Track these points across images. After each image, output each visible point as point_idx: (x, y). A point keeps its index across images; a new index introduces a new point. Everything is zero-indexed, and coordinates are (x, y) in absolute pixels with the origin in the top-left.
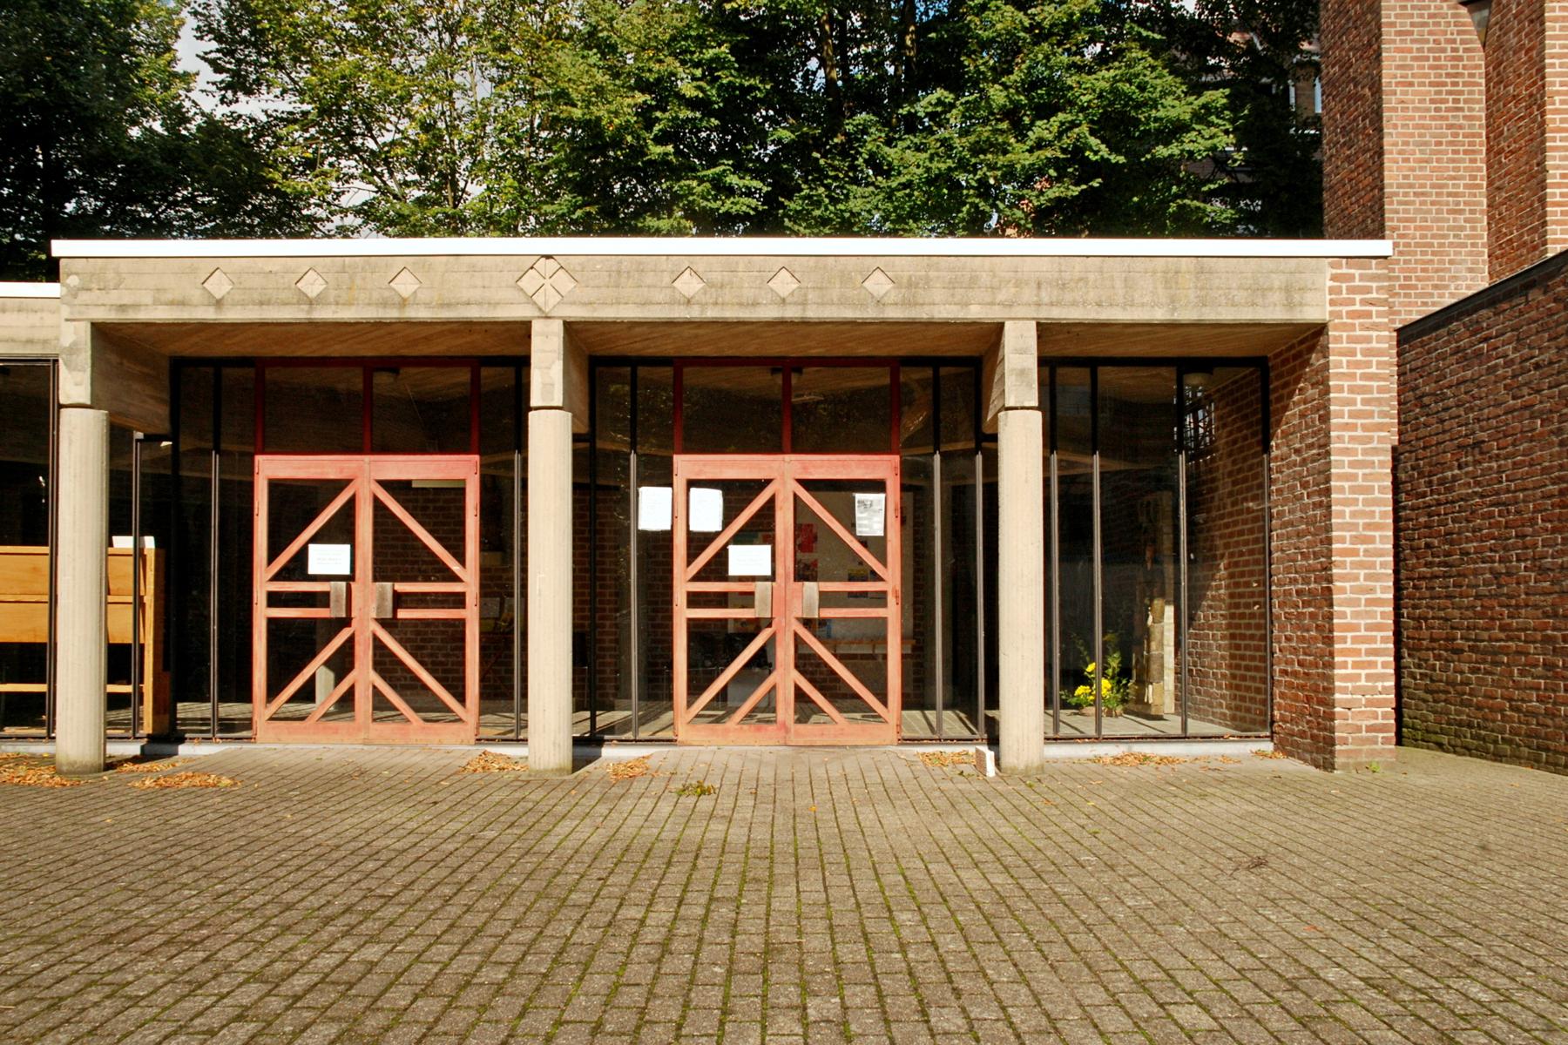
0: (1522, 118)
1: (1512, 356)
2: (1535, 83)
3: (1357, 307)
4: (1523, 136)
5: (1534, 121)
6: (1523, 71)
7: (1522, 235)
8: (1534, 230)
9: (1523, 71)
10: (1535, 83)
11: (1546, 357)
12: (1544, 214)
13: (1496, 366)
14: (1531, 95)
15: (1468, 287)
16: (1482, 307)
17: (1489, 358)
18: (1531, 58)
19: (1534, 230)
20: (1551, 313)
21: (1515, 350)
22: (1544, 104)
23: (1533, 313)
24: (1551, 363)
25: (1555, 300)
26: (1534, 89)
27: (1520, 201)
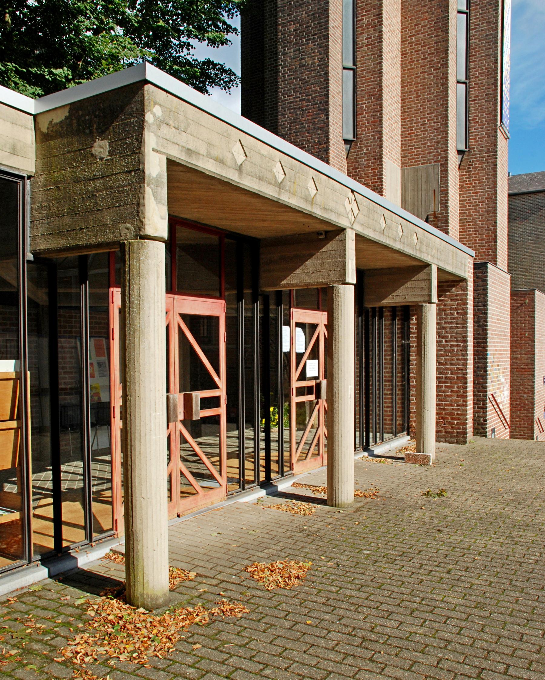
10: (377, 182)
26: (376, 184)
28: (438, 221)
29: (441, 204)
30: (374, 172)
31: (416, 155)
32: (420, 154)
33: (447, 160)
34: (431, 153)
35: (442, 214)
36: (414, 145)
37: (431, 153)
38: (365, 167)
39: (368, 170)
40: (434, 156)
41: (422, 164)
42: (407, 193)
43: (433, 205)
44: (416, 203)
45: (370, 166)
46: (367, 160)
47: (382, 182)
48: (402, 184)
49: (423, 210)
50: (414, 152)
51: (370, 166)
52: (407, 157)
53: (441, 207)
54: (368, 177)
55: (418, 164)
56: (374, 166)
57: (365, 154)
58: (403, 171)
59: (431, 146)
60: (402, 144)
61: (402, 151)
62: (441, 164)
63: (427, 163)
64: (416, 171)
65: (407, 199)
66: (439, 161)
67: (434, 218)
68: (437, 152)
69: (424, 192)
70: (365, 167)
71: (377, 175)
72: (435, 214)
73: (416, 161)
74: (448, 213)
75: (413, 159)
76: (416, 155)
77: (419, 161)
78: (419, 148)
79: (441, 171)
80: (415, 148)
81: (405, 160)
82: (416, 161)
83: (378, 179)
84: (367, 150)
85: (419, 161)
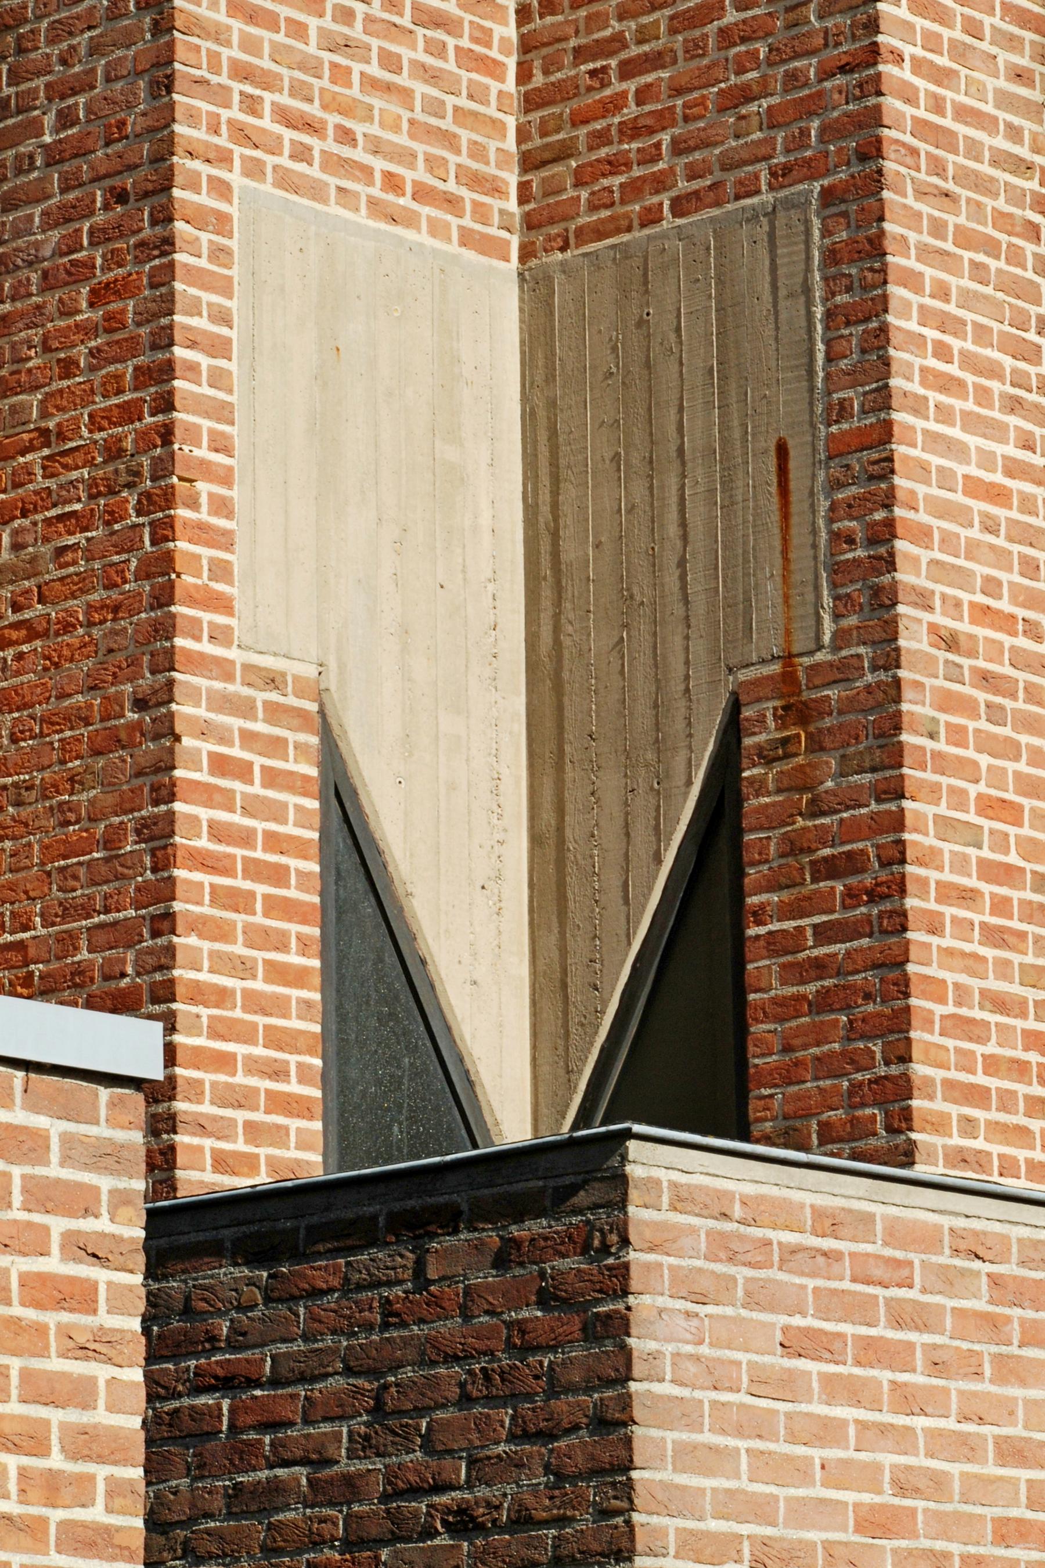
0: (80, 522)
1: (346, 1466)
2: (129, 413)
3: (53, 1264)
4: (81, 585)
5: (129, 546)
6: (81, 353)
7: (68, 942)
8: (122, 935)
9: (81, 353)
10: (129, 413)
11: (502, 1493)
12: (167, 890)
13: (275, 1487)
14: (114, 451)
15: (222, 1163)
16: (215, 1250)
17: (244, 1456)
18: (113, 323)
19: (122, 935)
20: (524, 1343)
21: (363, 1445)
22: (169, 498)
23: (449, 1327)
24: (523, 1521)
25: (544, 1300)
26: (128, 434)
27: (65, 814)
28: (816, 745)
29: (839, 571)
30: (113, 323)
31: (633, 130)
32: (663, 119)
33: (872, 151)
34: (746, 94)
35: (843, 672)
36: (618, 42)
37: (746, 94)
38: (48, 281)
39: (67, 311)
40: (772, 120)
41: (679, 207)
42: (569, 493)
43: (772, 589)
44: (642, 591)
45: (80, 272)
46: (66, 215)
47: (166, 404)
48: (529, 418)
49: (699, 648)
50: (617, 103)
51: (80, 272)
52: (563, 153)
53: (843, 604)
54: (68, 368)
55: (652, 217)
56: (114, 259)
57: (54, 156)
58: (535, 288)
59: (747, 33)
60: (527, 46)
61: (531, 102)
62: (828, 196)
63: (715, 195)
64: (638, 276)
65: (569, 552)
66: (811, 170)
67: (782, 720)
68: (793, 79)
69: (697, 472)
70: (48, 281)
71: (132, 347)
72: (788, 677)
73: (633, 190)
74: (891, 659)
75: (615, 165)
76: (633, 130)
77: (660, 182)
78: (655, 61)
79: (831, 257)
80: (627, 70)
81: (551, 189)
82: (633, 190)
83: (145, 376)
84: (66, 119)
85: (660, 182)
